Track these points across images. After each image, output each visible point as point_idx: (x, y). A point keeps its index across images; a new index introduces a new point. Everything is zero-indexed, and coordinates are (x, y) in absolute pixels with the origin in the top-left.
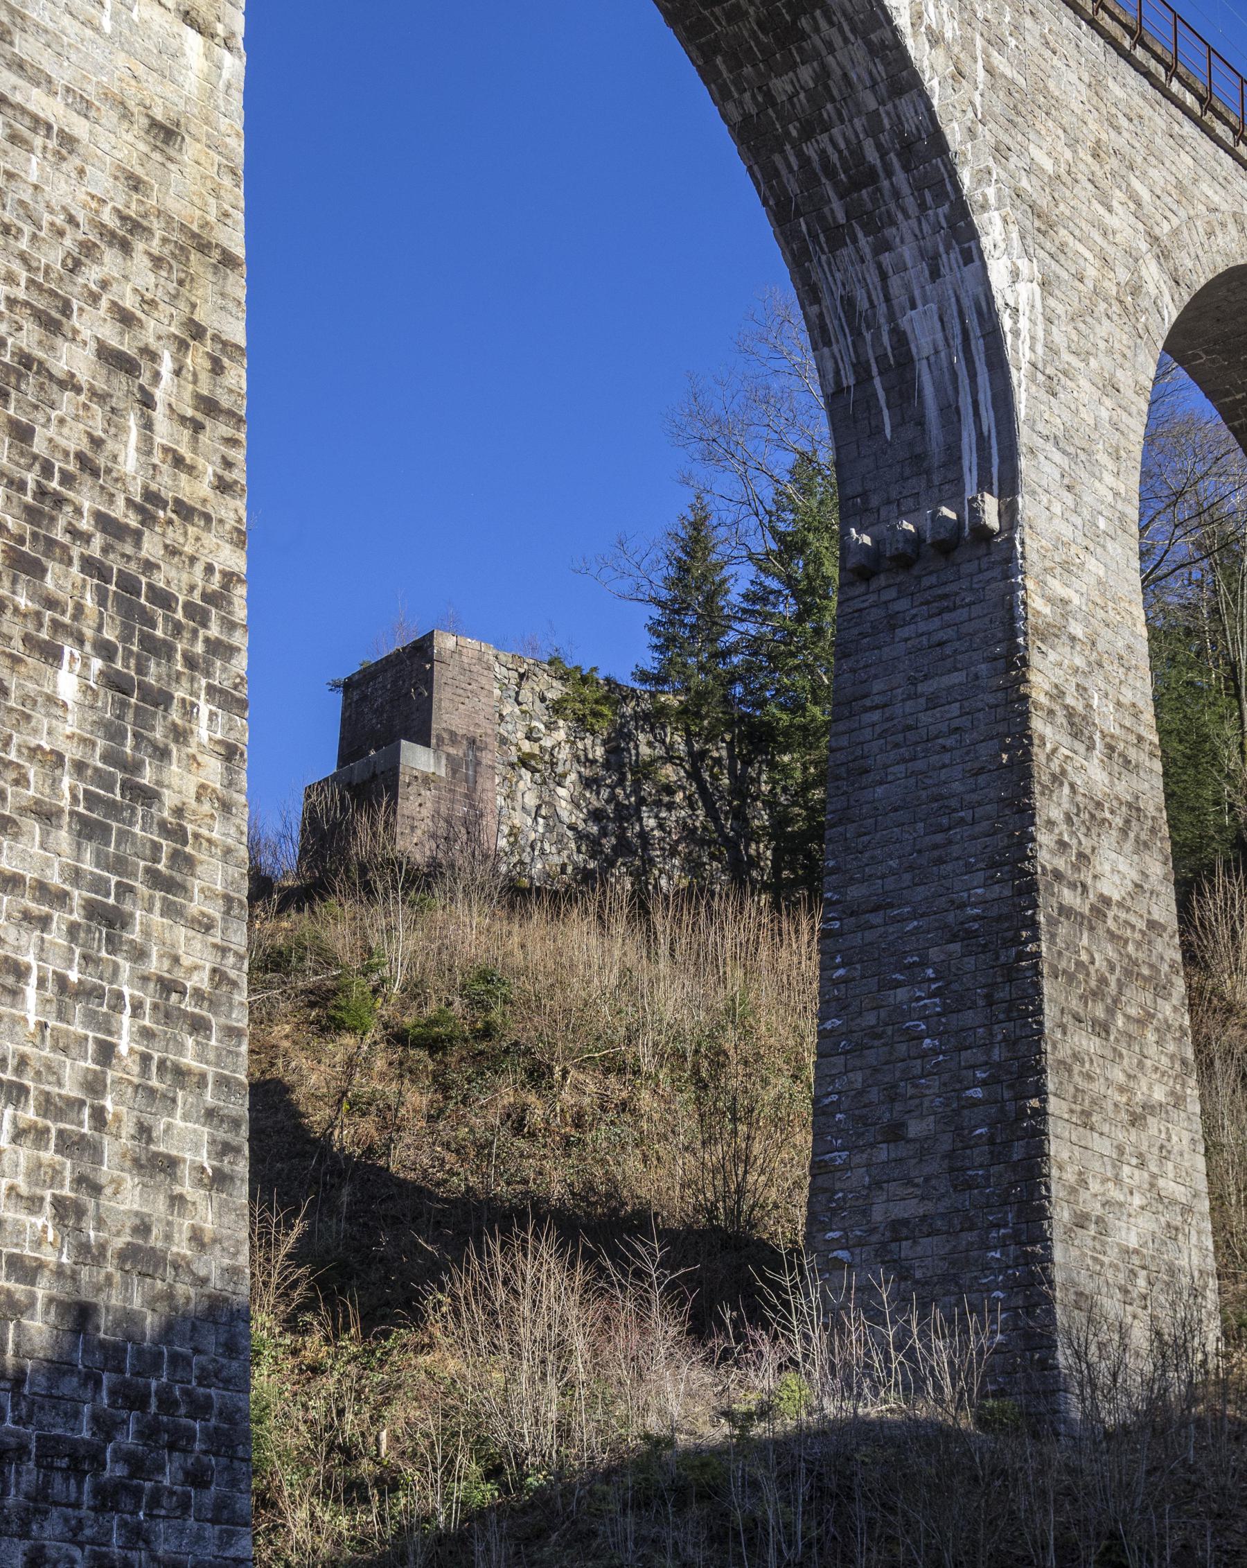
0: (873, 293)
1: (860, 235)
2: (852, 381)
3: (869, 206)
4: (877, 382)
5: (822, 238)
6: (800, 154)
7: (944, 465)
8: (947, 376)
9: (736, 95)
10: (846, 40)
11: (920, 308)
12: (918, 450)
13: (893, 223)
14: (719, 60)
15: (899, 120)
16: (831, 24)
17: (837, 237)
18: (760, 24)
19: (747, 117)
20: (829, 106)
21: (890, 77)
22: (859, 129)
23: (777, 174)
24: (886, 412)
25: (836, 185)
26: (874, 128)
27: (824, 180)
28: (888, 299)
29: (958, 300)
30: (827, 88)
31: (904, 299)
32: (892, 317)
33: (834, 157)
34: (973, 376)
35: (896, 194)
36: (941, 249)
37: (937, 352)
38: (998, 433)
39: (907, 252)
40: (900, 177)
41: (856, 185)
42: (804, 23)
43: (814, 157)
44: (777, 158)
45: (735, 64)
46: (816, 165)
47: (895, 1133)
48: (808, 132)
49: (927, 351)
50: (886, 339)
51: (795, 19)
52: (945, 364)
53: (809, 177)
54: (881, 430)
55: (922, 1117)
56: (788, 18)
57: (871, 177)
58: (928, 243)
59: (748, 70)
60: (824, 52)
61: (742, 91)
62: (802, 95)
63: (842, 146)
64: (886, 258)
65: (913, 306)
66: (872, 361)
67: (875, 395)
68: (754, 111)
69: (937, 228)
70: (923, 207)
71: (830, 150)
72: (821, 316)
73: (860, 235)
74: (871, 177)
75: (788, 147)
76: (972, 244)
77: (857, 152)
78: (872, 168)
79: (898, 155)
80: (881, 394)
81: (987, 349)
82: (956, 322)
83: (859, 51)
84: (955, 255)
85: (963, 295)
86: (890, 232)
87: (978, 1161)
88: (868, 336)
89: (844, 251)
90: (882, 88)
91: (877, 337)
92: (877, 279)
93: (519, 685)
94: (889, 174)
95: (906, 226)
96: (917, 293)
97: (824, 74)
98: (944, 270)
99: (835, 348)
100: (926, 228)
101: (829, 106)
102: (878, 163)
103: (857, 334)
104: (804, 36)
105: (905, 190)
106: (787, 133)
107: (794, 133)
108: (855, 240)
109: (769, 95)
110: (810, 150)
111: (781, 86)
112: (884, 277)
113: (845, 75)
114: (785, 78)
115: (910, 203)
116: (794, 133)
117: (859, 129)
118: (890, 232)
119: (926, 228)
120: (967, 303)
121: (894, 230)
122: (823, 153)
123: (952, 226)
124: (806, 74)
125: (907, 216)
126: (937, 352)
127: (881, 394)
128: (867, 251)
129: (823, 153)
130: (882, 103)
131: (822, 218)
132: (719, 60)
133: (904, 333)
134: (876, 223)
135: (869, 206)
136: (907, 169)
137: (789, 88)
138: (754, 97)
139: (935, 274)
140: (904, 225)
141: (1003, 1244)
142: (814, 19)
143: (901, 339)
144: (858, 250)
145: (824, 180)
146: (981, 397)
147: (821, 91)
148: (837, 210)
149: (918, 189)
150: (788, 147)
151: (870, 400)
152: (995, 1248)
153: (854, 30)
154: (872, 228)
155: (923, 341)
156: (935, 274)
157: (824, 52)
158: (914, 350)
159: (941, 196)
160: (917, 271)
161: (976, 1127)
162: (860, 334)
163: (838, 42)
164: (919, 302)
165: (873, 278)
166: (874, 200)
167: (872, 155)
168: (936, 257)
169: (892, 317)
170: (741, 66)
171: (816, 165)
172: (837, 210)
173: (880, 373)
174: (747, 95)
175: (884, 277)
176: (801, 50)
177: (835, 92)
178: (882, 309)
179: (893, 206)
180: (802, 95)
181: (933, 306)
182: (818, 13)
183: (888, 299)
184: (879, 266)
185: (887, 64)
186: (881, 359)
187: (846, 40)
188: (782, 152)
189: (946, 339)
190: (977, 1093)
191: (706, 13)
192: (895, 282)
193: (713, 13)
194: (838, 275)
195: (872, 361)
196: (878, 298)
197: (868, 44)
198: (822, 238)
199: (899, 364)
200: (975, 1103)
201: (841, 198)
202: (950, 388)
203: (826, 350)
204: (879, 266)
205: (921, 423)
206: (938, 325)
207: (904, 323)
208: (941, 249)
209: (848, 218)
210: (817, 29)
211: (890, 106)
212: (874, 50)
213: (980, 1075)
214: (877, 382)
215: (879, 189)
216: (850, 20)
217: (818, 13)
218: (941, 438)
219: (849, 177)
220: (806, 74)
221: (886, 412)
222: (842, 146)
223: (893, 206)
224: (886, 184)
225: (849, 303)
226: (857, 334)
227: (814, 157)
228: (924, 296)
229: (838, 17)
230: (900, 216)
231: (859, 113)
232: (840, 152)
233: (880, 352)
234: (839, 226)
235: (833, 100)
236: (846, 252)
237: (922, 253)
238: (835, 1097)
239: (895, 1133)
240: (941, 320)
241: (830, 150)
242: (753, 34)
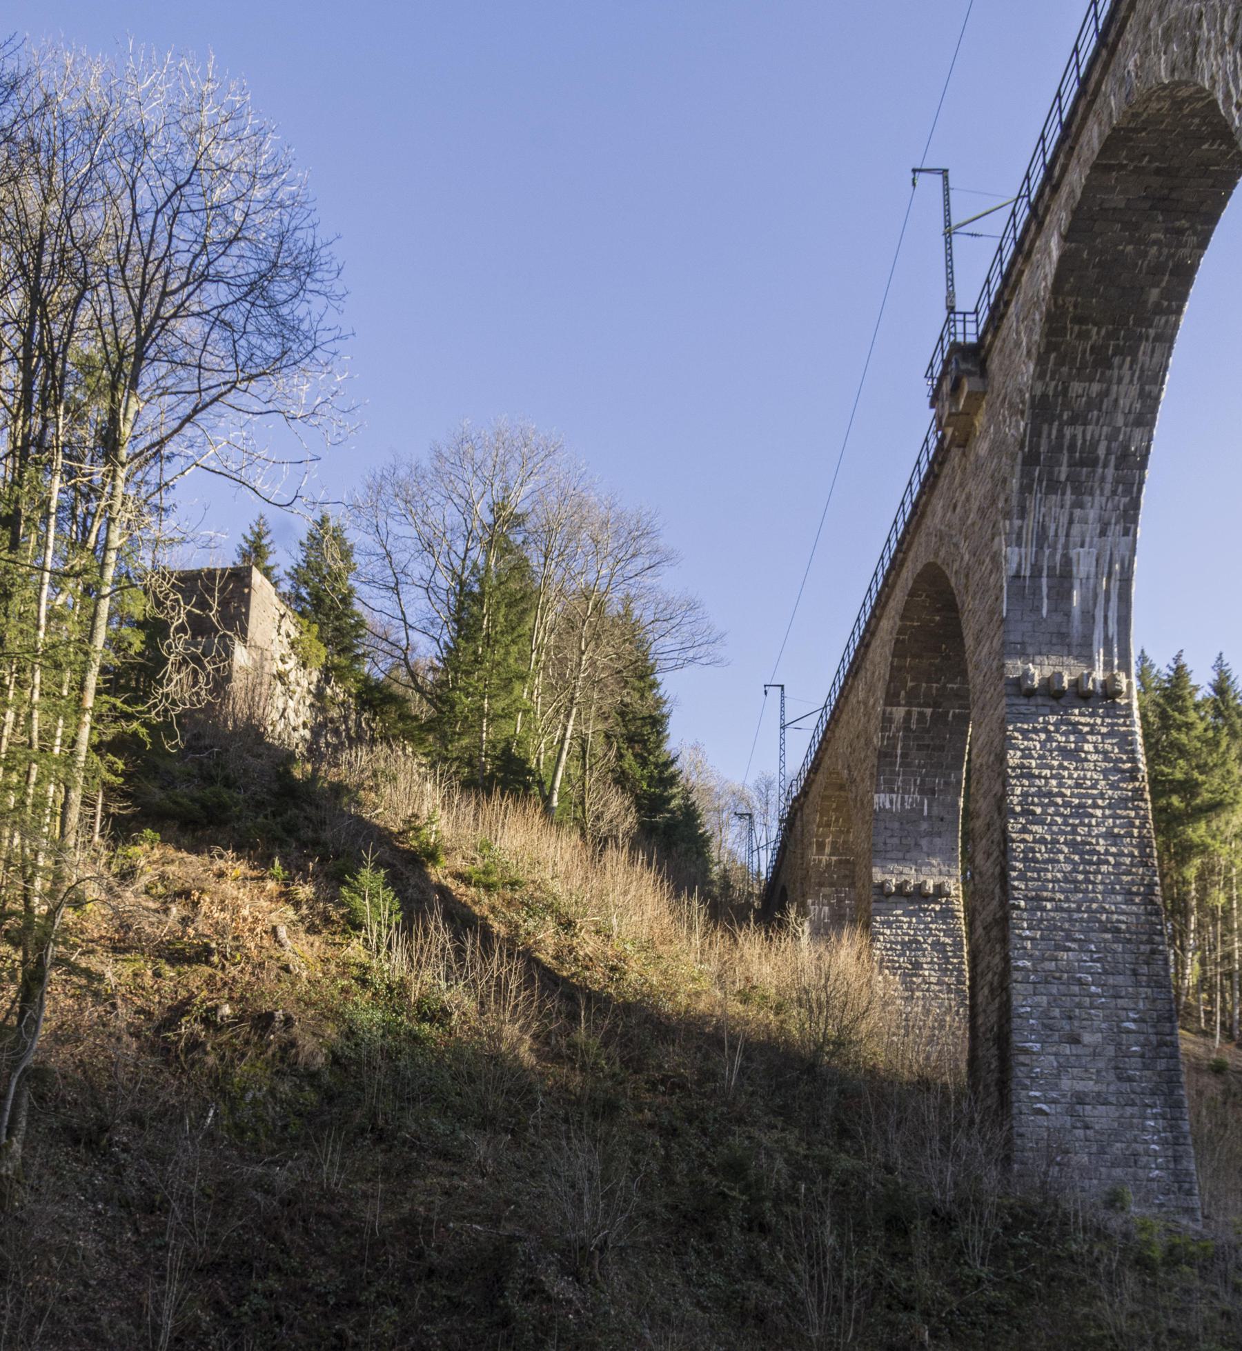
0: (1060, 530)
1: (1069, 492)
2: (1028, 574)
3: (1083, 478)
4: (1044, 581)
5: (1044, 484)
6: (1060, 431)
7: (1080, 645)
8: (1091, 594)
9: (1048, 379)
10: (1131, 381)
11: (1086, 548)
12: (1064, 630)
13: (1092, 494)
14: (1053, 356)
15: (1129, 439)
16: (1131, 368)
17: (1054, 486)
18: (1092, 348)
19: (1044, 395)
20: (1095, 413)
21: (1140, 414)
22: (1104, 433)
23: (1039, 436)
24: (1045, 601)
25: (1071, 457)
26: (1111, 438)
27: (1065, 452)
28: (1067, 535)
29: (1111, 554)
30: (1101, 402)
31: (1078, 540)
32: (1066, 546)
33: (1079, 443)
34: (1107, 600)
35: (1103, 479)
36: (1113, 521)
37: (1088, 578)
38: (1119, 639)
39: (1092, 514)
40: (1110, 472)
41: (1082, 463)
42: (1116, 361)
43: (1068, 436)
44: (1045, 427)
45: (1060, 363)
46: (1066, 442)
47: (1075, 1040)
48: (1073, 421)
49: (1083, 575)
50: (1058, 557)
51: (1114, 355)
52: (1091, 586)
53: (1057, 448)
54: (1039, 609)
55: (1093, 1032)
56: (1110, 352)
57: (1093, 462)
58: (1107, 515)
59: (1065, 369)
60: (1115, 381)
61: (1052, 379)
62: (1084, 399)
63: (1088, 438)
64: (1077, 512)
65: (1082, 546)
66: (1045, 568)
67: (1040, 588)
68: (1051, 393)
69: (1116, 508)
70: (1114, 493)
71: (1080, 437)
72: (1021, 528)
73: (1069, 492)
74: (1093, 462)
75: (1056, 423)
76: (1133, 526)
77: (1095, 445)
78: (1097, 458)
79: (1117, 458)
80: (1045, 590)
81: (1120, 588)
82: (1106, 565)
83: (1134, 390)
84: (1119, 528)
85: (1115, 552)
86: (1087, 498)
87: (1134, 1066)
88: (1047, 552)
89: (1054, 497)
90: (1132, 417)
91: (1053, 555)
92: (1066, 522)
93: (280, 621)
94: (1105, 466)
95: (1099, 500)
96: (1088, 539)
97: (1105, 394)
98: (1110, 533)
99: (1023, 550)
100: (1110, 505)
101: (1095, 413)
102: (1102, 457)
103: (1040, 547)
104: (1110, 367)
105: (1109, 478)
106: (1061, 415)
107: (1065, 417)
108: (1063, 494)
109: (1065, 390)
110: (1068, 431)
111: (1076, 387)
112: (1071, 522)
113: (1116, 400)
114: (1082, 384)
115: (1108, 488)
116: (1065, 417)
117: (1104, 433)
118: (1087, 498)
119: (1110, 505)
120: (1117, 557)
121: (1090, 499)
122: (1074, 437)
123: (1125, 511)
124: (1096, 388)
125: (1102, 494)
126: (1088, 578)
127: (1045, 590)
128: (1068, 503)
129: (1074, 437)
130: (1126, 425)
131: (1051, 473)
132: (1053, 356)
133: (1070, 560)
134: (1080, 489)
135: (1083, 478)
136: (1117, 468)
137: (1080, 391)
138: (1057, 386)
139: (1103, 533)
140: (1097, 498)
141: (1155, 1117)
142: (1124, 361)
143: (1067, 561)
144: (1062, 500)
145: (1065, 452)
146: (1110, 614)
147: (1094, 403)
148: (1063, 472)
149: (1117, 481)
150: (1056, 423)
151: (1036, 591)
152: (1150, 1119)
153: (1140, 378)
154: (1077, 491)
155: (1082, 568)
156: (1103, 533)
157: (1115, 381)
158: (1075, 569)
159: (1127, 492)
160: (1093, 528)
161: (1132, 1045)
162: (1042, 548)
163: (1126, 380)
164: (1087, 545)
165: (1064, 520)
166: (1088, 476)
167: (1101, 451)
168: (1108, 524)
169: (1066, 546)
170: (1063, 365)
171: (1066, 442)
172: (1063, 472)
173: (1048, 576)
174: (1053, 383)
175: (1071, 522)
176: (1103, 374)
177: (1104, 407)
178: (1062, 540)
179: (1096, 485)
180: (1084, 399)
181: (1094, 551)
182: (1129, 359)
183: (1067, 535)
184: (1071, 514)
185: (1143, 406)
186: (1051, 569)
187: (1131, 381)
188: (1051, 425)
189: (1097, 573)
190: (1132, 1026)
191: (1069, 326)
192: (1076, 529)
193: (1072, 329)
194: (1043, 509)
195: (1045, 568)
196: (1062, 533)
197: (1142, 389)
198: (1044, 484)
199: (1061, 576)
200: (1129, 1031)
201: (1070, 466)
202: (1091, 603)
203: (1016, 549)
204: (1071, 514)
205: (1068, 614)
206: (1094, 563)
207: (1073, 553)
208: (1113, 521)
209: (1067, 479)
210: (1120, 367)
211: (1129, 429)
212: (1142, 395)
213: (1131, 1015)
214: (1044, 581)
215: (1094, 472)
216: (1142, 370)
217: (1129, 359)
218: (1080, 629)
219: (1081, 457)
220: (1096, 388)
221: (1045, 601)
222: (1088, 438)
223: (1096, 485)
224: (1100, 470)
225: (1044, 529)
226: (1040, 547)
227: (1068, 436)
228: (1091, 541)
229: (1138, 368)
230: (1098, 492)
231: (1109, 425)
232: (1084, 440)
233: (1051, 564)
234: (1058, 482)
235: (1100, 410)
236: (1054, 499)
237: (1100, 519)
238: (1029, 1009)
239: (1075, 1040)
240: (1097, 560)
241: (1080, 437)
242: (1084, 352)
